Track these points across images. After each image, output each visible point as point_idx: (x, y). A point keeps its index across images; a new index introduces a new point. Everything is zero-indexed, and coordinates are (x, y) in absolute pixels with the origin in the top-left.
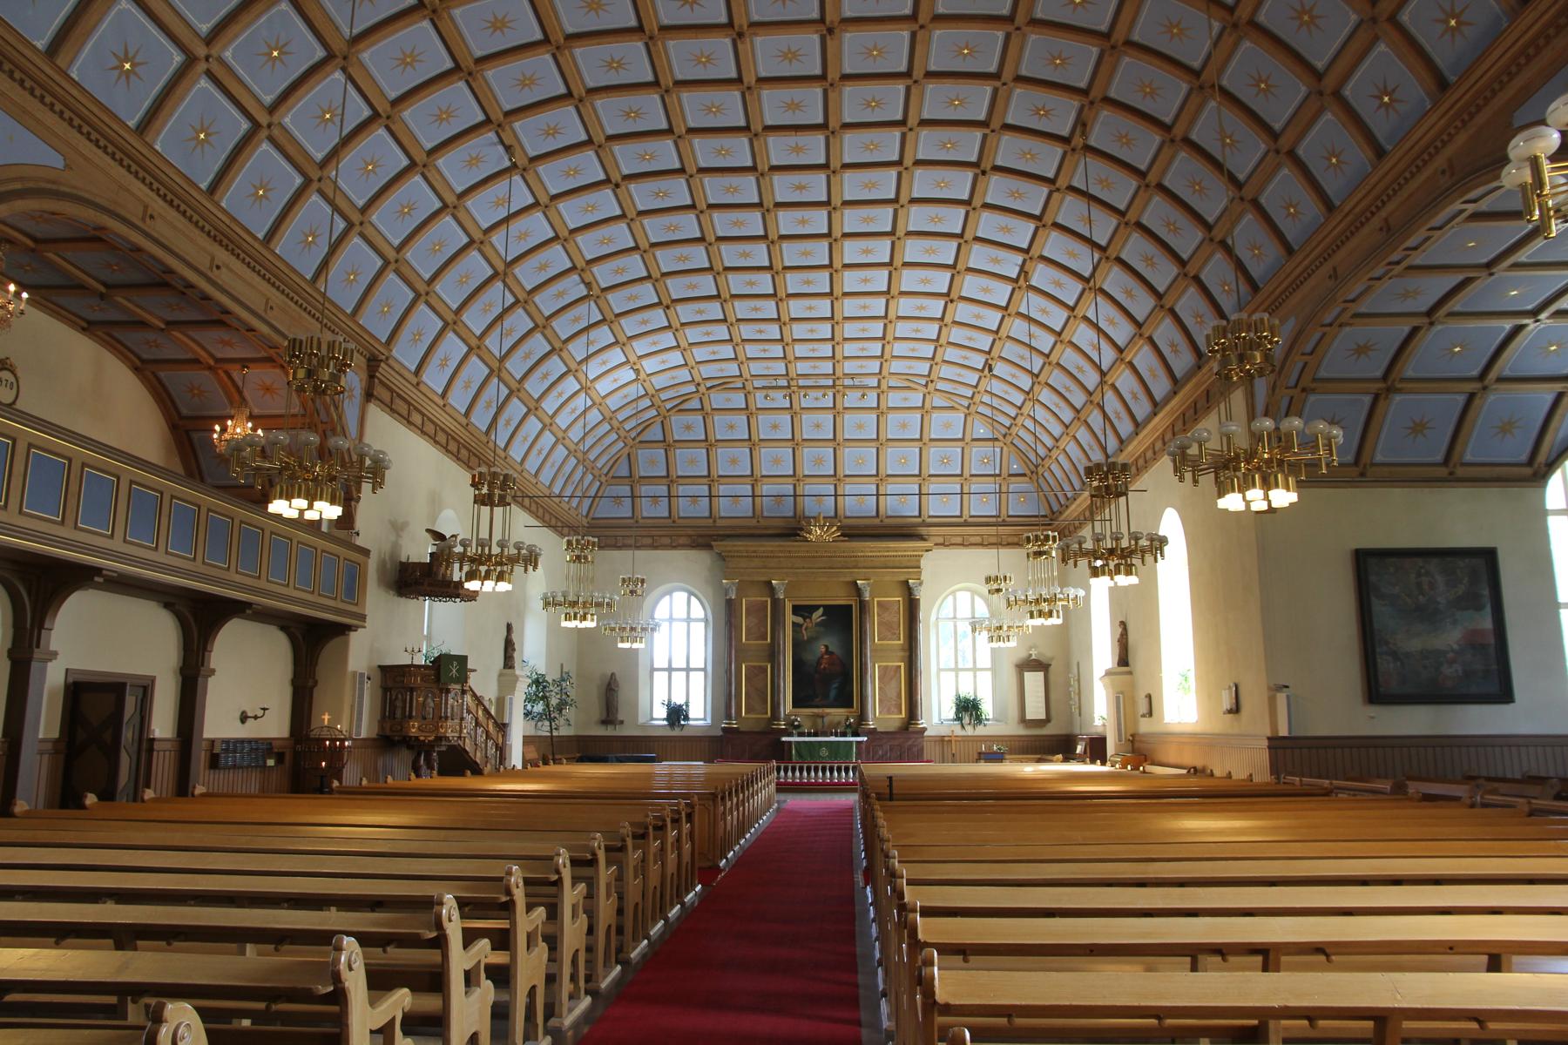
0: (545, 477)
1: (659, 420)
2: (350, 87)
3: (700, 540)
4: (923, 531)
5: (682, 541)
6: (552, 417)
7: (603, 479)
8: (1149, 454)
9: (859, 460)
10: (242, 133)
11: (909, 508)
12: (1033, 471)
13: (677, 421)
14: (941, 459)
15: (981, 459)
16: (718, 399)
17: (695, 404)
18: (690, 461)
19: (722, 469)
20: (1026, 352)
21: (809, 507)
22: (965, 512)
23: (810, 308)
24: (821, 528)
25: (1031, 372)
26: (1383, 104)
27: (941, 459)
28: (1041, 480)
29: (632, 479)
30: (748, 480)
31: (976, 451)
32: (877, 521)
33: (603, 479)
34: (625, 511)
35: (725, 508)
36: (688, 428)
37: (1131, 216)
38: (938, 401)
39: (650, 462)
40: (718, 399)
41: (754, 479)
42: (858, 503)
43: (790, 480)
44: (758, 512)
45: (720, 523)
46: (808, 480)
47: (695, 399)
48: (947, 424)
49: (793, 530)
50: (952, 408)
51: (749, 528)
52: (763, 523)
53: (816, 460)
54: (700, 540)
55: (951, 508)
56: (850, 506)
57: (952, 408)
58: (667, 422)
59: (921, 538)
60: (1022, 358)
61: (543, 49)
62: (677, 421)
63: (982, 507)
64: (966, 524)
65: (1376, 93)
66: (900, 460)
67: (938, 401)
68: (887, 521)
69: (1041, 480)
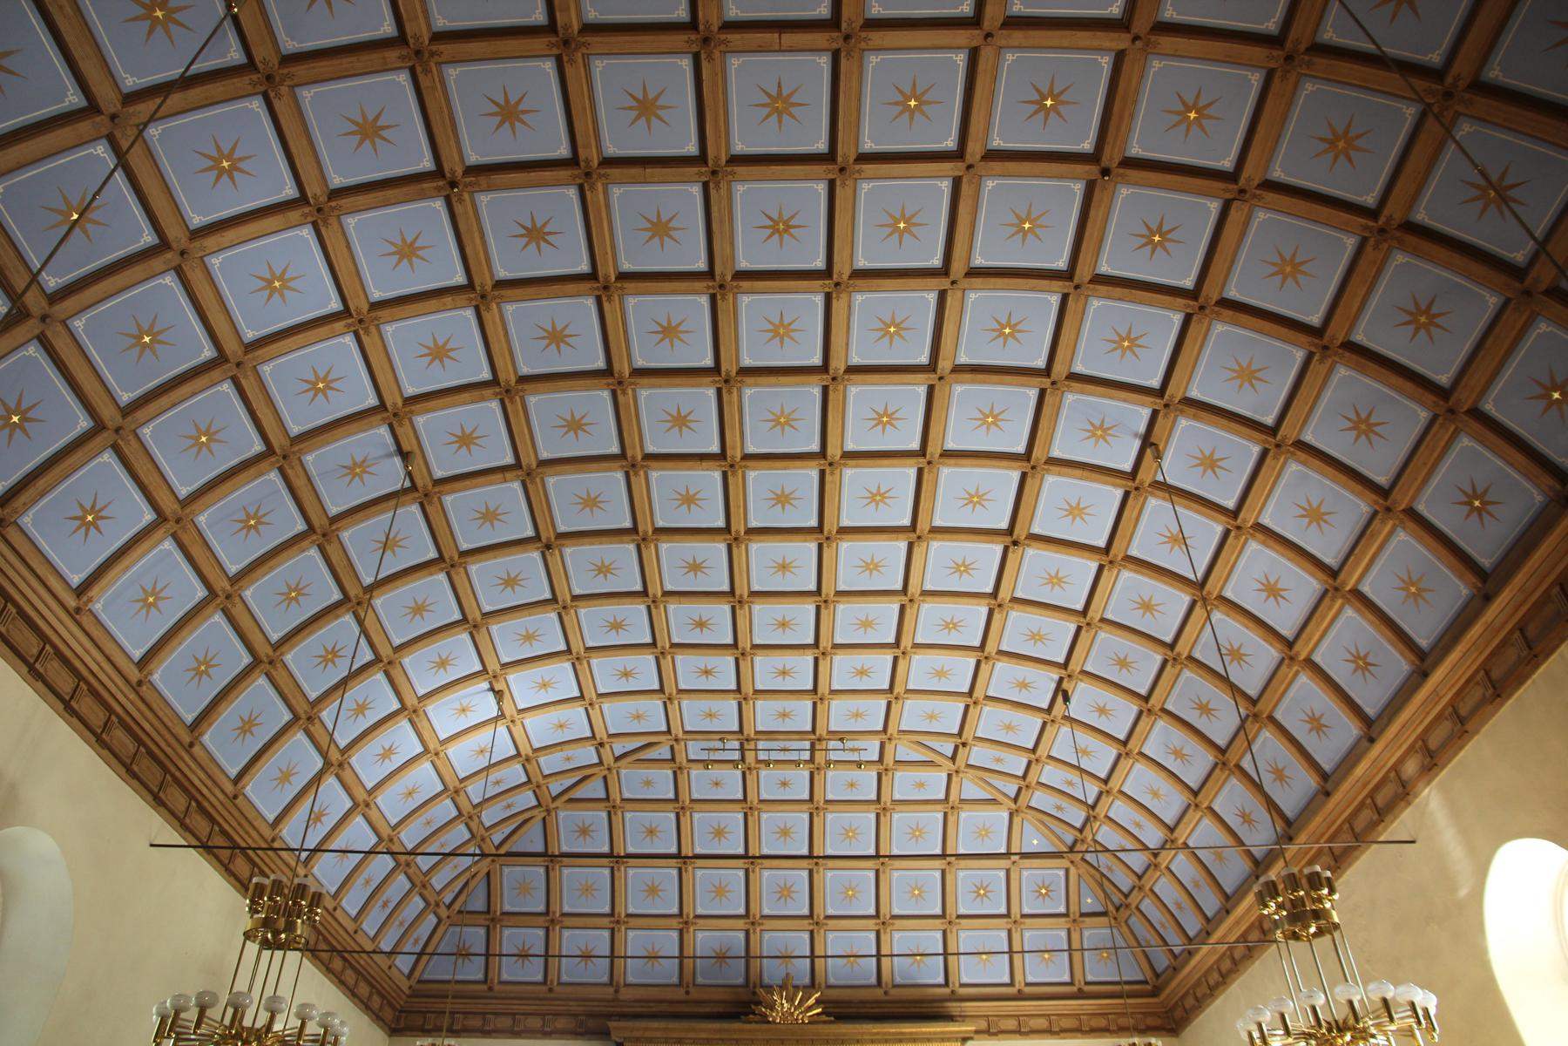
0: (370, 926)
1: (539, 814)
2: (363, 641)
3: (591, 1023)
4: (954, 1008)
5: (561, 1023)
6: (370, 792)
7: (443, 912)
8: (1226, 965)
9: (846, 890)
10: (242, 666)
11: (932, 973)
12: (1117, 908)
13: (566, 818)
14: (978, 889)
15: (1043, 887)
16: (632, 781)
17: (594, 789)
18: (583, 889)
19: (634, 903)
20: (1074, 777)
21: (772, 972)
22: (1018, 977)
23: (784, 715)
24: (791, 1000)
25: (1085, 803)
26: (1474, 509)
27: (978, 889)
28: (1135, 921)
29: (492, 919)
30: (674, 922)
31: (1029, 874)
32: (879, 993)
33: (443, 912)
34: (473, 971)
35: (634, 972)
36: (584, 831)
37: (1394, 210)
38: (971, 789)
39: (521, 887)
40: (632, 781)
41: (684, 921)
42: (849, 954)
43: (741, 923)
44: (688, 977)
45: (625, 994)
46: (768, 924)
47: (598, 780)
48: (982, 828)
49: (744, 1004)
50: (993, 801)
51: (671, 1002)
52: (695, 994)
53: (782, 891)
54: (591, 1023)
55: (996, 971)
56: (835, 972)
57: (993, 801)
58: (551, 820)
59: (950, 1018)
60: (1070, 783)
61: (549, 607)
62: (566, 818)
63: (1050, 971)
64: (1020, 996)
65: (1541, 391)
66: (913, 890)
67: (970, 788)
68: (895, 993)
69: (1135, 921)
